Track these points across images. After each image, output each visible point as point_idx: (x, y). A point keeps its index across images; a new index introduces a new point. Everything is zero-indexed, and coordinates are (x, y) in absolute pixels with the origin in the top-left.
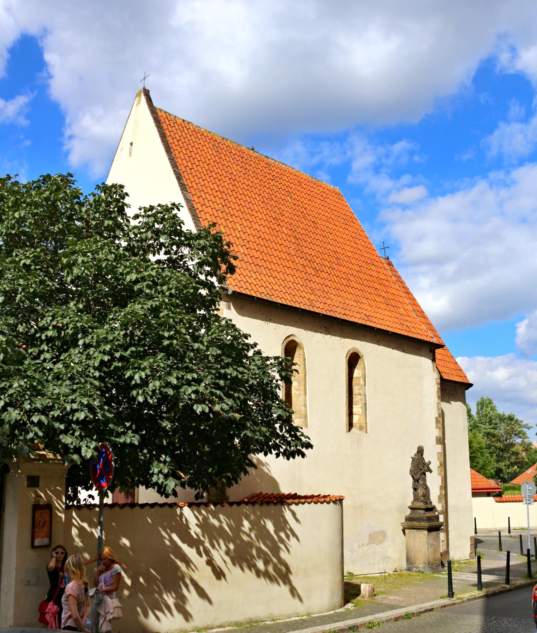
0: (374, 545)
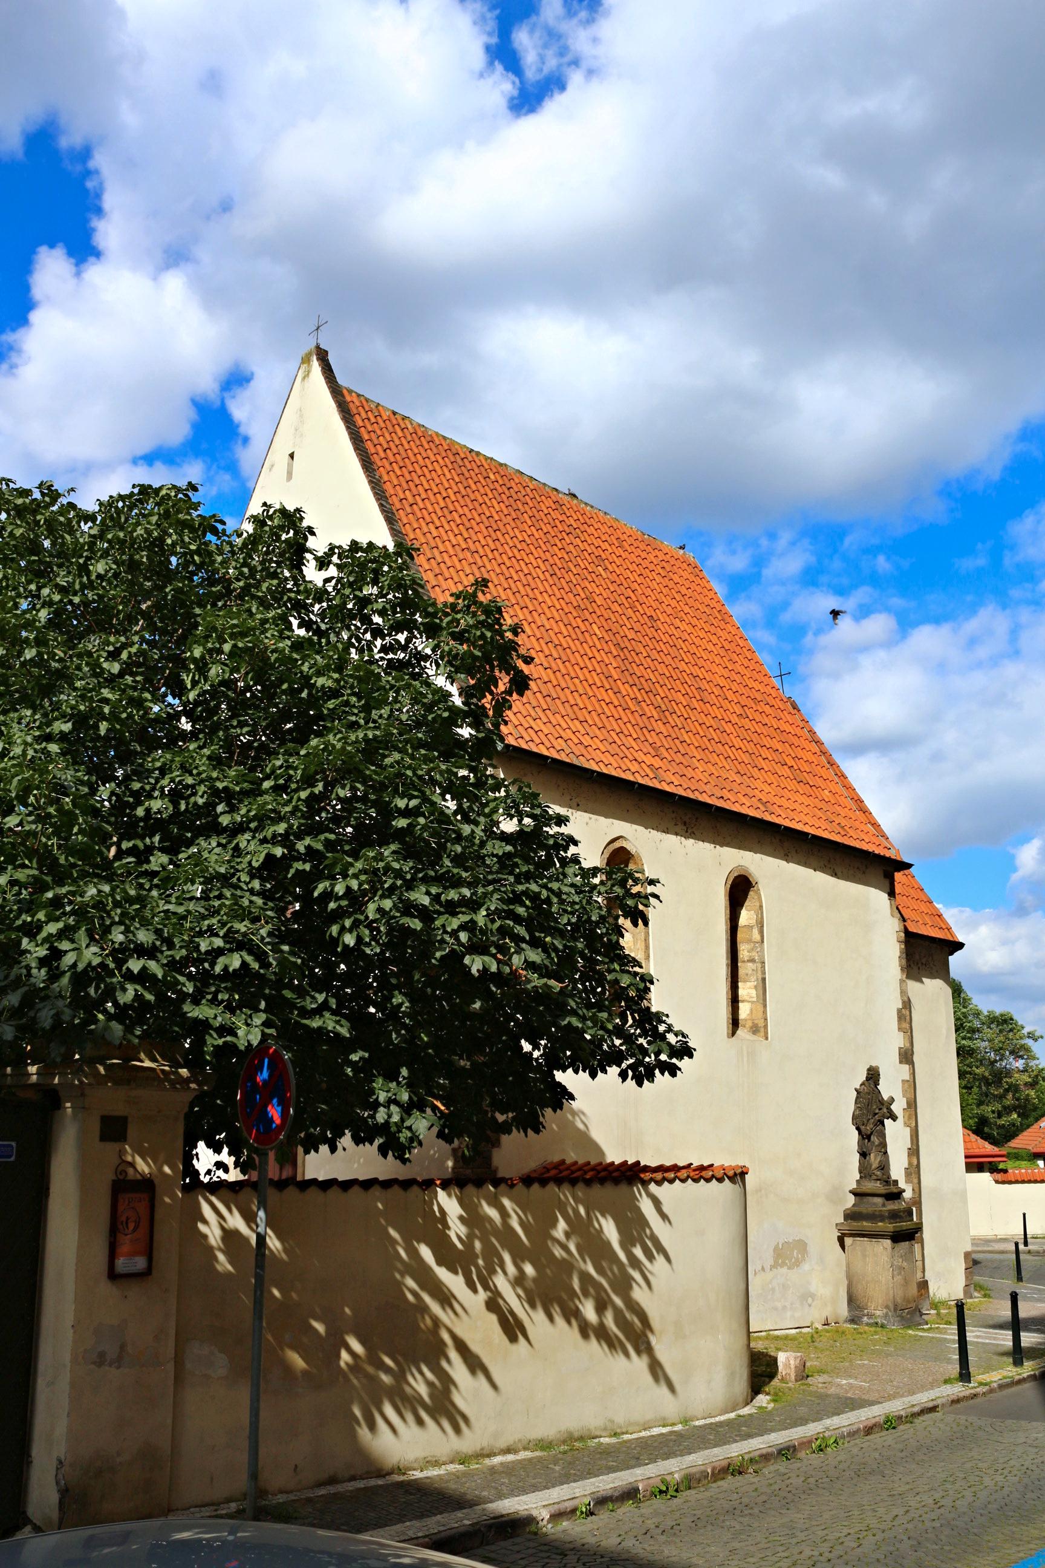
0: (784, 1270)
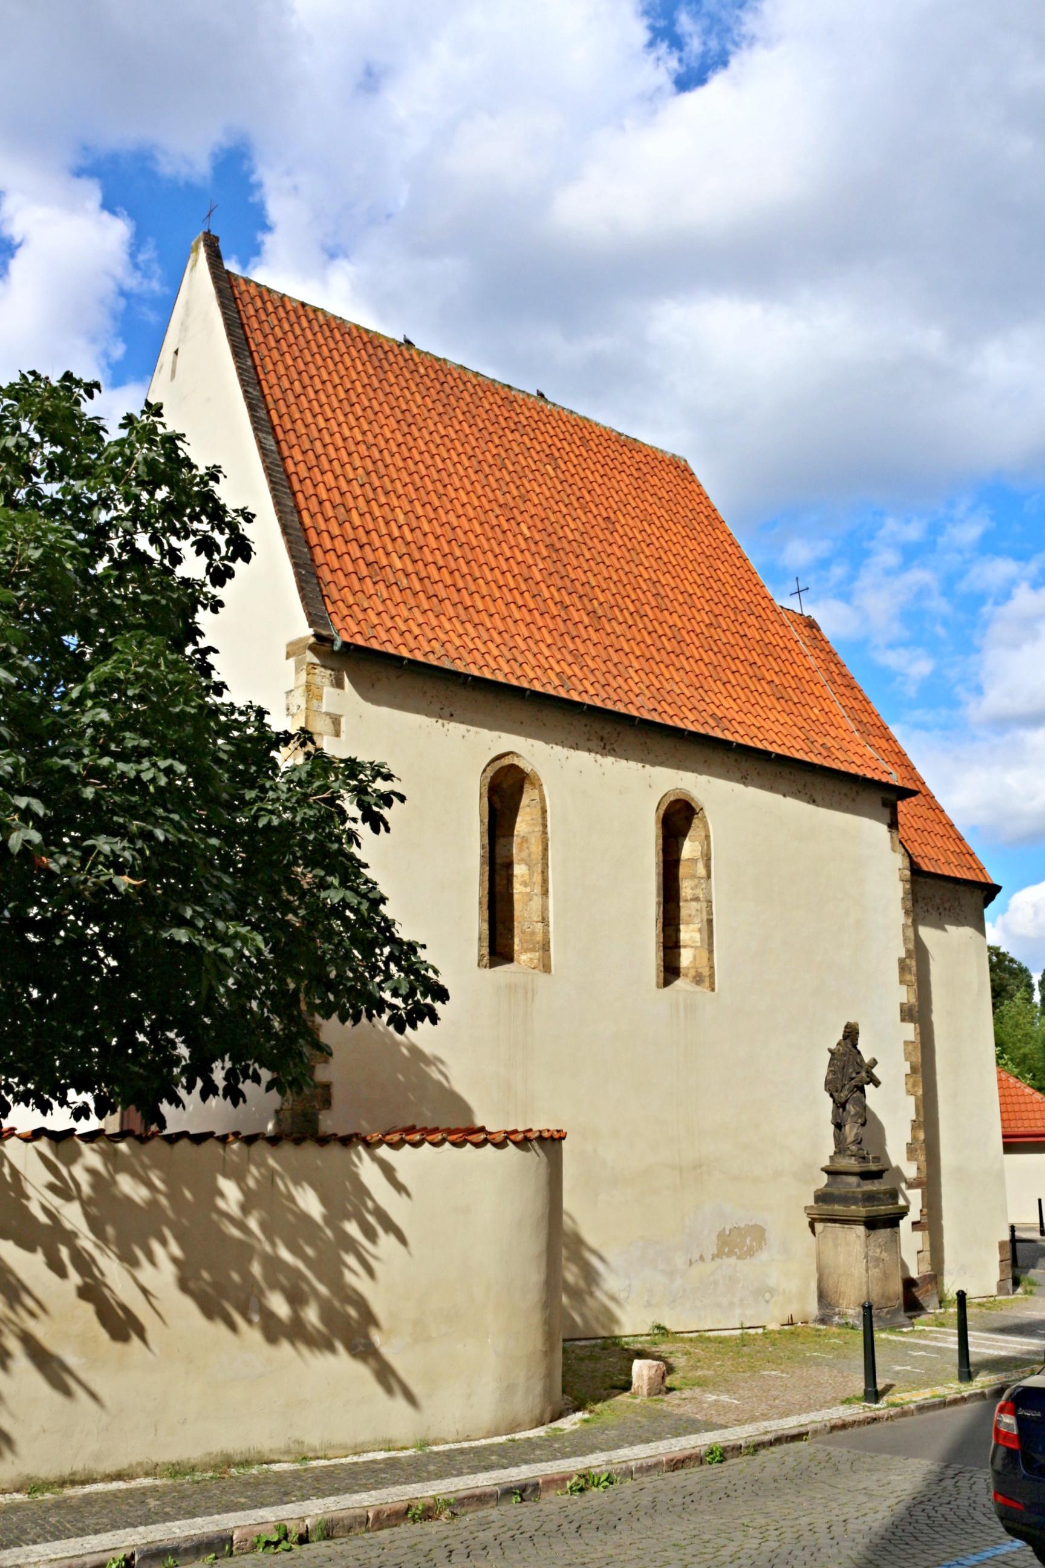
0: (733, 1260)
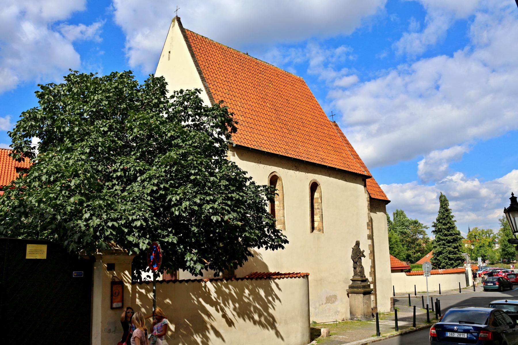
0: (330, 304)
